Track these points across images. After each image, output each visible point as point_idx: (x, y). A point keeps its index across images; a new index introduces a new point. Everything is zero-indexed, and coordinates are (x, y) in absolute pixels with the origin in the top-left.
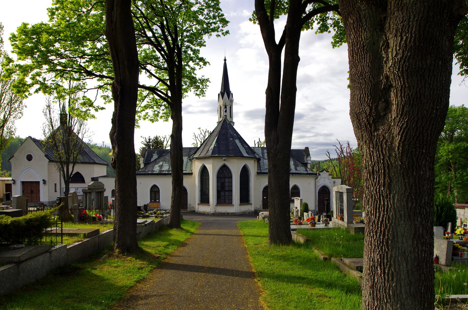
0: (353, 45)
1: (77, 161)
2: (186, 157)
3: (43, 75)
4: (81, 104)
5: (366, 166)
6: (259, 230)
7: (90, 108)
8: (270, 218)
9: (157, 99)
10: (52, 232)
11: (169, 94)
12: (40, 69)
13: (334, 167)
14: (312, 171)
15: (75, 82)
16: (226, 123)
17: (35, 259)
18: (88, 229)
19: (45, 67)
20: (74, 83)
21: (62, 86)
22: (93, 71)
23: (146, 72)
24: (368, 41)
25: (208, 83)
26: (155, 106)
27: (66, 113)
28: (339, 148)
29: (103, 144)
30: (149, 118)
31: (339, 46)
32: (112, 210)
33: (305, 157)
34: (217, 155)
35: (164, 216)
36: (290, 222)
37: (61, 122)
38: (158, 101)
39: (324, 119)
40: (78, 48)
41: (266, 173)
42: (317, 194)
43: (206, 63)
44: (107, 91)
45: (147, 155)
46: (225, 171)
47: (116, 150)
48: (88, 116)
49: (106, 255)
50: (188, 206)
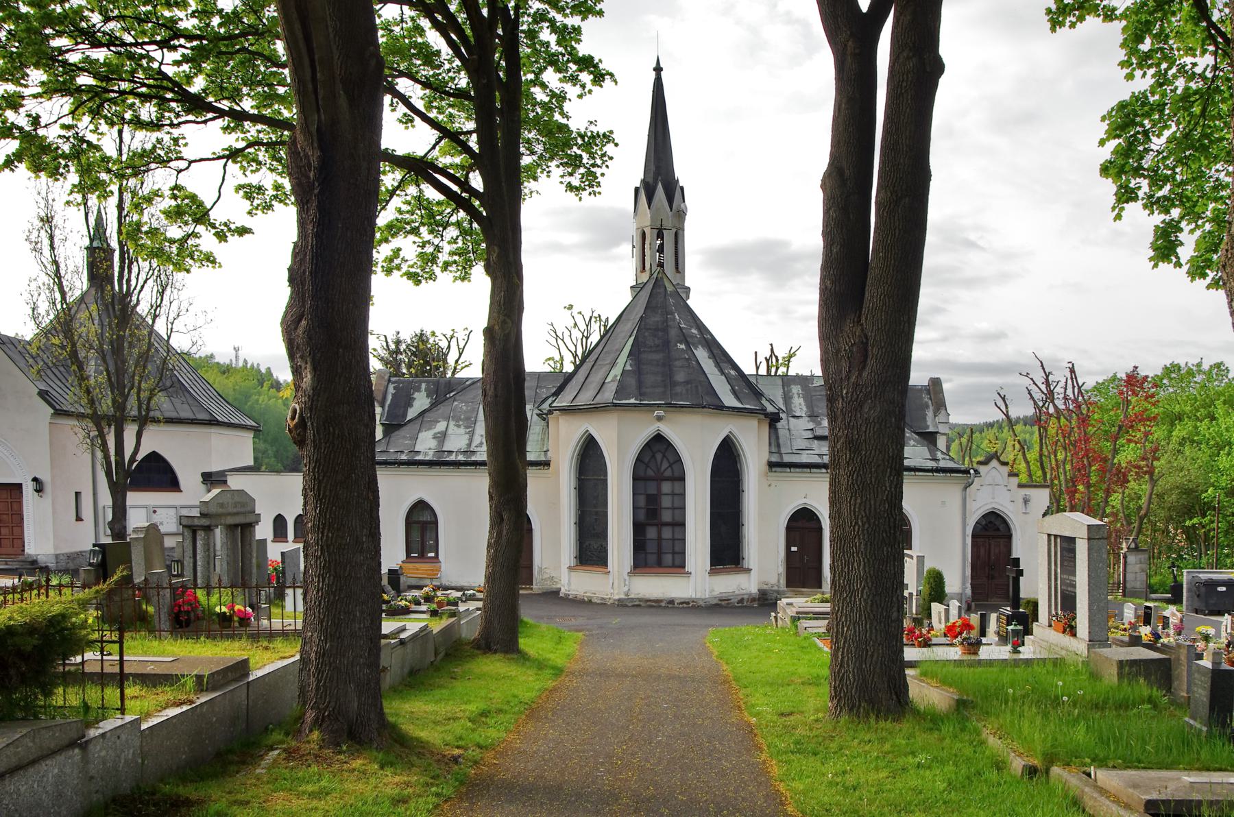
1: (152, 414)
3: (30, 105)
4: (168, 214)
7: (200, 229)
10: (88, 669)
12: (17, 82)
15: (141, 134)
16: (662, 290)
17: (31, 770)
18: (210, 661)
19: (37, 76)
20: (140, 140)
21: (98, 148)
22: (207, 95)
25: (609, 149)
26: (422, 224)
27: (108, 245)
29: (237, 357)
30: (405, 268)
31: (1073, 25)
33: (930, 413)
34: (632, 401)
37: (92, 277)
39: (971, 283)
40: (150, 12)
42: (969, 540)
43: (603, 76)
44: (257, 170)
46: (659, 456)
47: (308, 378)
48: (192, 258)
49: (276, 752)
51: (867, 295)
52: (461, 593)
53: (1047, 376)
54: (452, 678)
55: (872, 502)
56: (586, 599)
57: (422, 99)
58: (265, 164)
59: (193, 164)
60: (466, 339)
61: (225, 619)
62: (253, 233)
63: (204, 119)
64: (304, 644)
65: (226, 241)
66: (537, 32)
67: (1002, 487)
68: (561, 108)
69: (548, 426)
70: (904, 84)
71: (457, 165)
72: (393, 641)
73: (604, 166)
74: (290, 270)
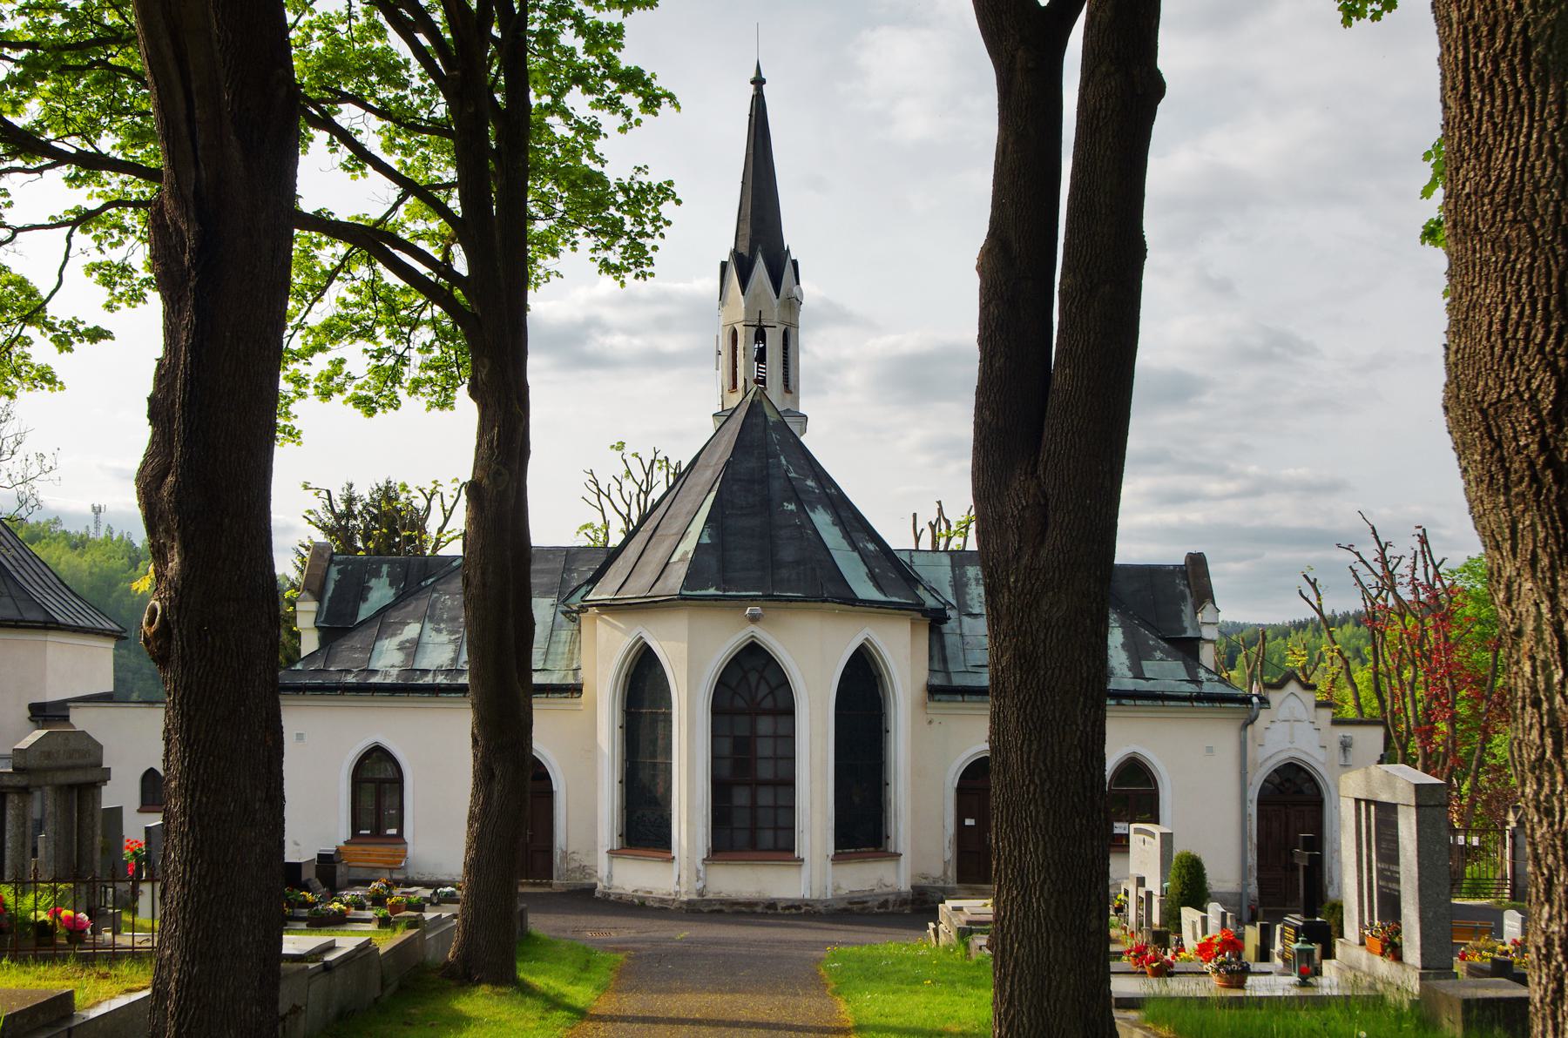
0: (1465, 36)
2: (549, 601)
5: (1534, 689)
6: (939, 999)
7: (31, 331)
8: (1002, 933)
9: (391, 290)
11: (461, 265)
13: (1346, 662)
14: (1222, 681)
22: (44, 129)
23: (331, 143)
24: (1552, 15)
25: (667, 208)
26: (380, 324)
28: (1369, 559)
29: (97, 522)
30: (350, 390)
31: (1376, 16)
32: (145, 888)
33: (1188, 609)
34: (712, 591)
35: (429, 915)
36: (1107, 957)
38: (401, 299)
41: (979, 692)
42: (1253, 809)
43: (657, 98)
44: (120, 243)
45: (338, 584)
46: (753, 678)
47: (174, 563)
48: (18, 375)
50: (557, 859)
51: (1047, 433)
52: (431, 891)
53: (1383, 550)
54: (405, 1023)
55: (1056, 749)
56: (636, 901)
57: (380, 133)
58: (134, 232)
59: (19, 235)
60: (456, 496)
61: (44, 931)
62: (113, 338)
63: (38, 165)
64: (161, 967)
65: (70, 350)
66: (555, 34)
67: (1307, 723)
68: (590, 148)
69: (580, 631)
70: (1103, 114)
71: (434, 234)
72: (311, 966)
73: (657, 234)
74: (151, 400)
